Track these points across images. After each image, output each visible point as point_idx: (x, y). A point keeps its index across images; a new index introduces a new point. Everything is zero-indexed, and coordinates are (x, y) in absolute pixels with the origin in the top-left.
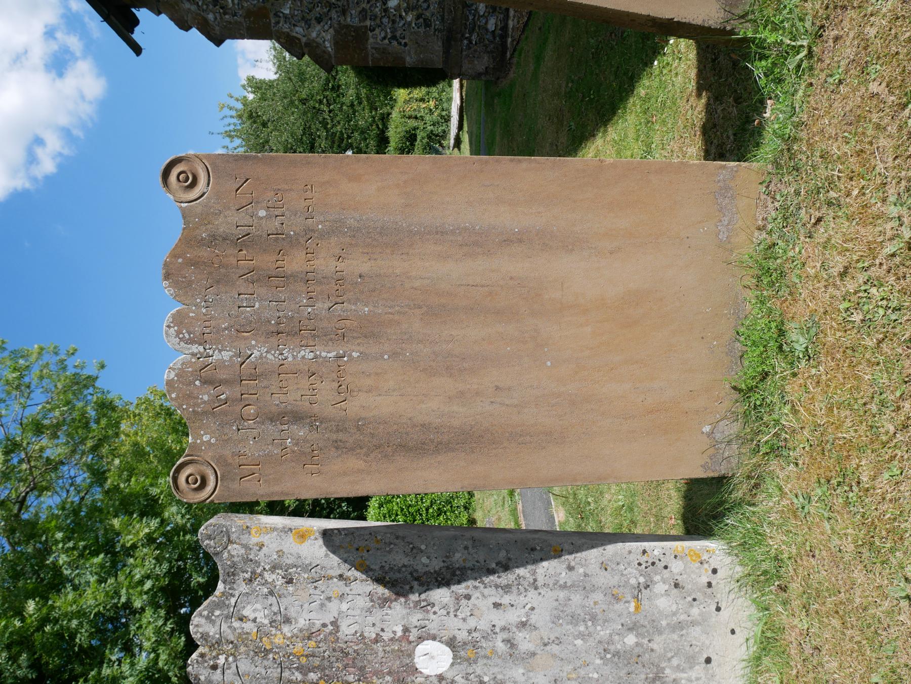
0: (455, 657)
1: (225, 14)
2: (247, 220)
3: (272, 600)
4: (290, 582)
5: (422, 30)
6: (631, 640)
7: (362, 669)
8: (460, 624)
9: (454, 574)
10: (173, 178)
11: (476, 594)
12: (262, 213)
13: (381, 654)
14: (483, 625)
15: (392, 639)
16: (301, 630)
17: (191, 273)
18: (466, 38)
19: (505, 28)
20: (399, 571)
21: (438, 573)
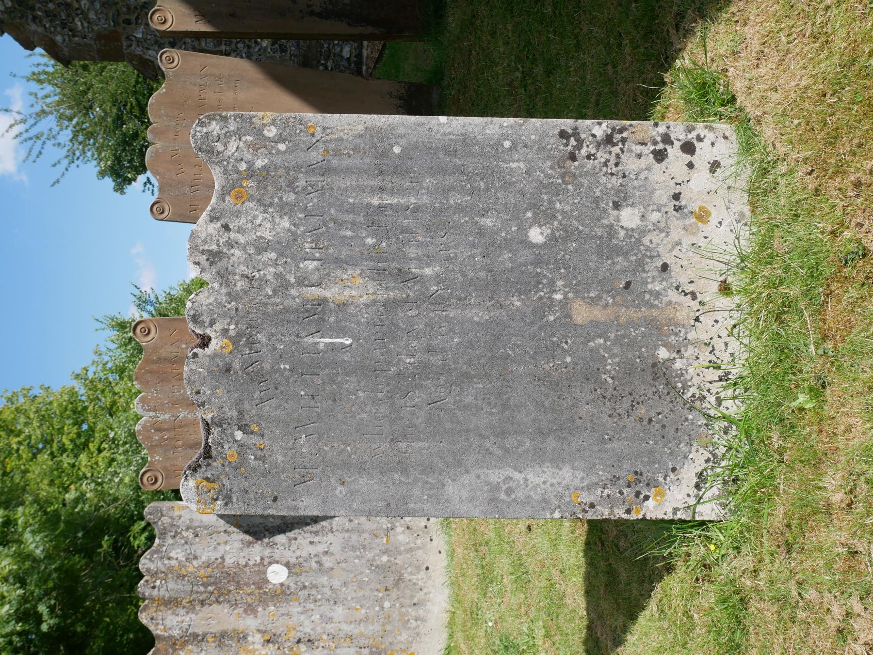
0: (289, 573)
1: (74, 36)
2: (176, 350)
3: (187, 547)
4: (197, 536)
5: (278, 55)
6: (385, 558)
7: (238, 582)
8: (292, 554)
9: (288, 527)
10: (138, 330)
11: (300, 537)
12: (184, 346)
13: (248, 573)
14: (304, 554)
15: (254, 565)
16: (203, 563)
17: (148, 377)
18: (322, 64)
19: (359, 56)
20: (258, 526)
21: (279, 526)
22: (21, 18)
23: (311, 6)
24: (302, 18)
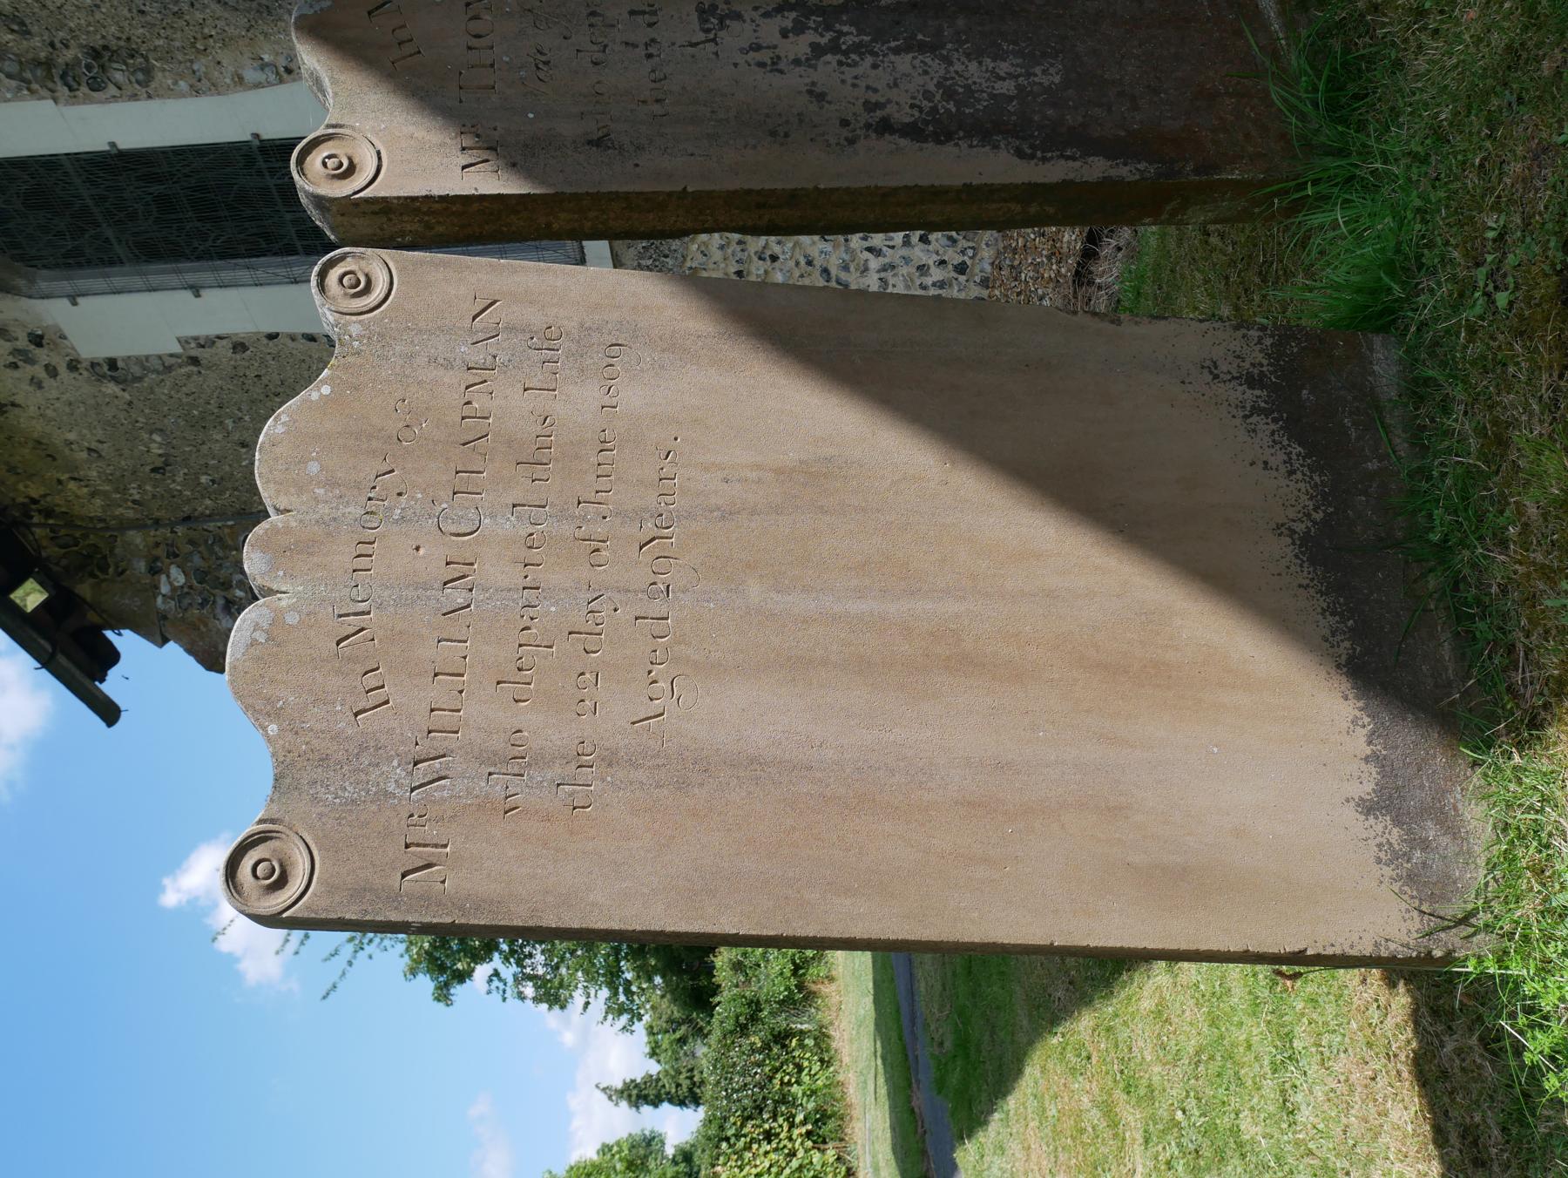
22: (202, 605)
23: (878, 106)
24: (851, 142)
